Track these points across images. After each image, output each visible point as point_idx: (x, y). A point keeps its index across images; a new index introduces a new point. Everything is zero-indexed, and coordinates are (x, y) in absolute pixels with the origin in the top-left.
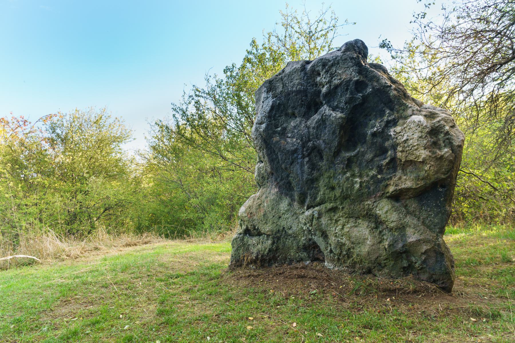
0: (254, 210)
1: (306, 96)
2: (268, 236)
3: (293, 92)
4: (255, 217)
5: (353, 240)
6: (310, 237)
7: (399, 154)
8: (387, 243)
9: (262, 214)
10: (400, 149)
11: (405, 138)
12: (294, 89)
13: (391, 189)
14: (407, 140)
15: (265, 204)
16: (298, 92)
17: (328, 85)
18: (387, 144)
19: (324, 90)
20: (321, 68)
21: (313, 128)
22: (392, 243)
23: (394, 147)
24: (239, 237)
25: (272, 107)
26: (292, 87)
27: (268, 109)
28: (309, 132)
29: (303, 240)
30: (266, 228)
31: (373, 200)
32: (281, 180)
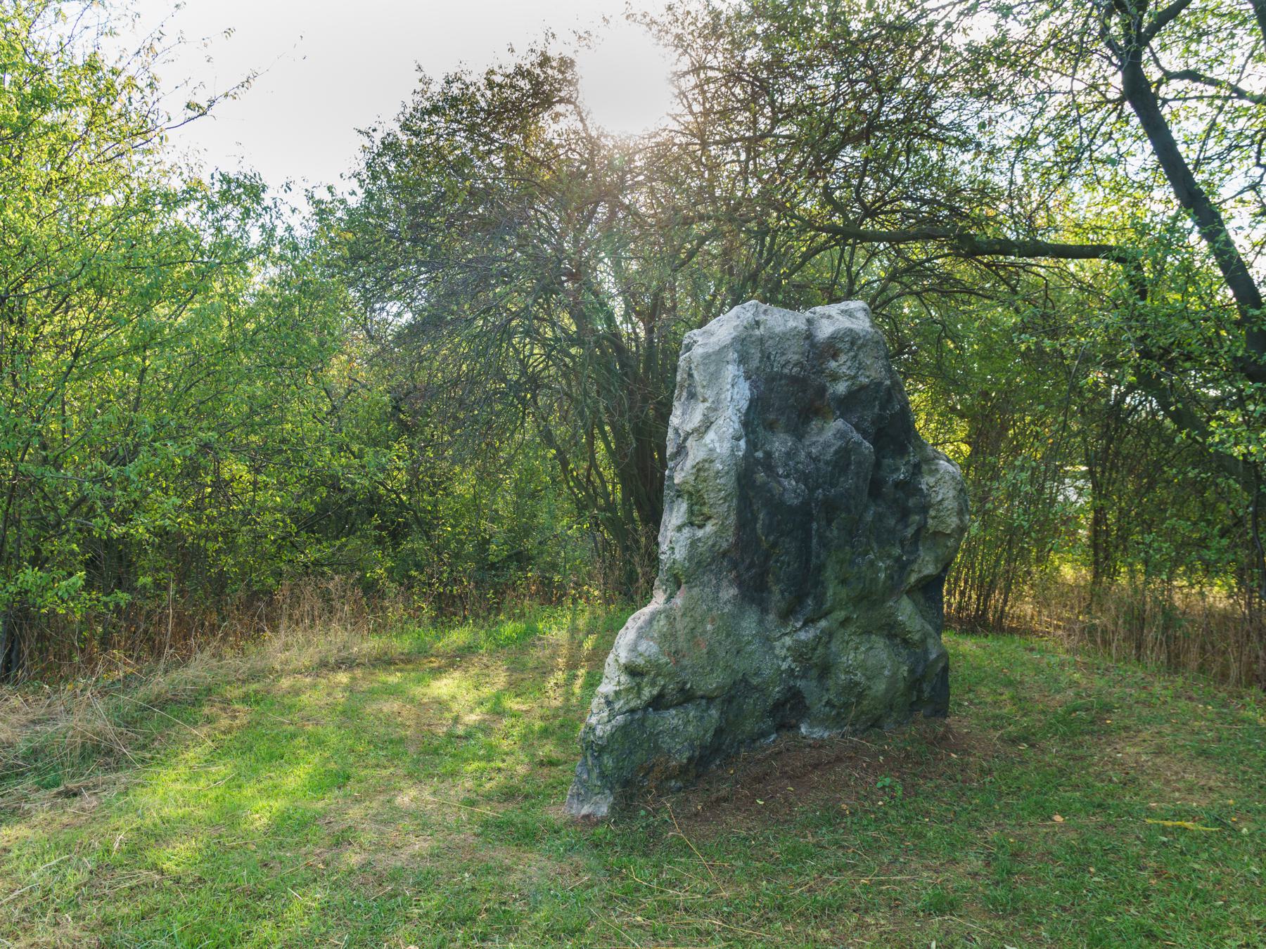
0: (682, 643)
1: (804, 391)
2: (710, 700)
3: (782, 376)
4: (686, 662)
5: (868, 673)
6: (792, 683)
7: (930, 521)
8: (906, 668)
9: (705, 651)
10: (932, 513)
11: (940, 498)
12: (786, 371)
13: (913, 578)
14: (943, 500)
15: (709, 627)
16: (794, 380)
17: (849, 383)
18: (911, 502)
19: (841, 388)
20: (847, 346)
21: (827, 463)
22: (385, 697)
23: (924, 509)
24: (631, 722)
25: (753, 402)
26: (783, 366)
27: (745, 407)
28: (818, 469)
29: (776, 691)
30: (713, 682)
31: (895, 598)
32: (748, 569)
